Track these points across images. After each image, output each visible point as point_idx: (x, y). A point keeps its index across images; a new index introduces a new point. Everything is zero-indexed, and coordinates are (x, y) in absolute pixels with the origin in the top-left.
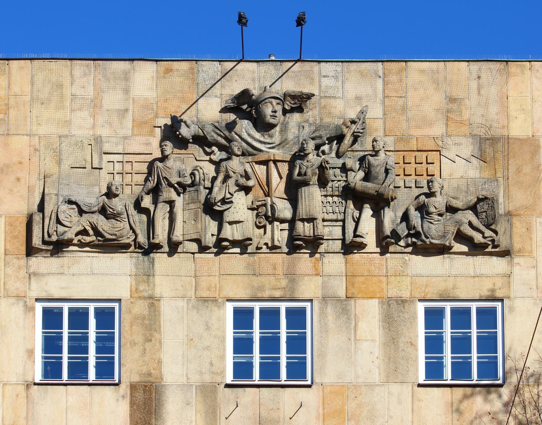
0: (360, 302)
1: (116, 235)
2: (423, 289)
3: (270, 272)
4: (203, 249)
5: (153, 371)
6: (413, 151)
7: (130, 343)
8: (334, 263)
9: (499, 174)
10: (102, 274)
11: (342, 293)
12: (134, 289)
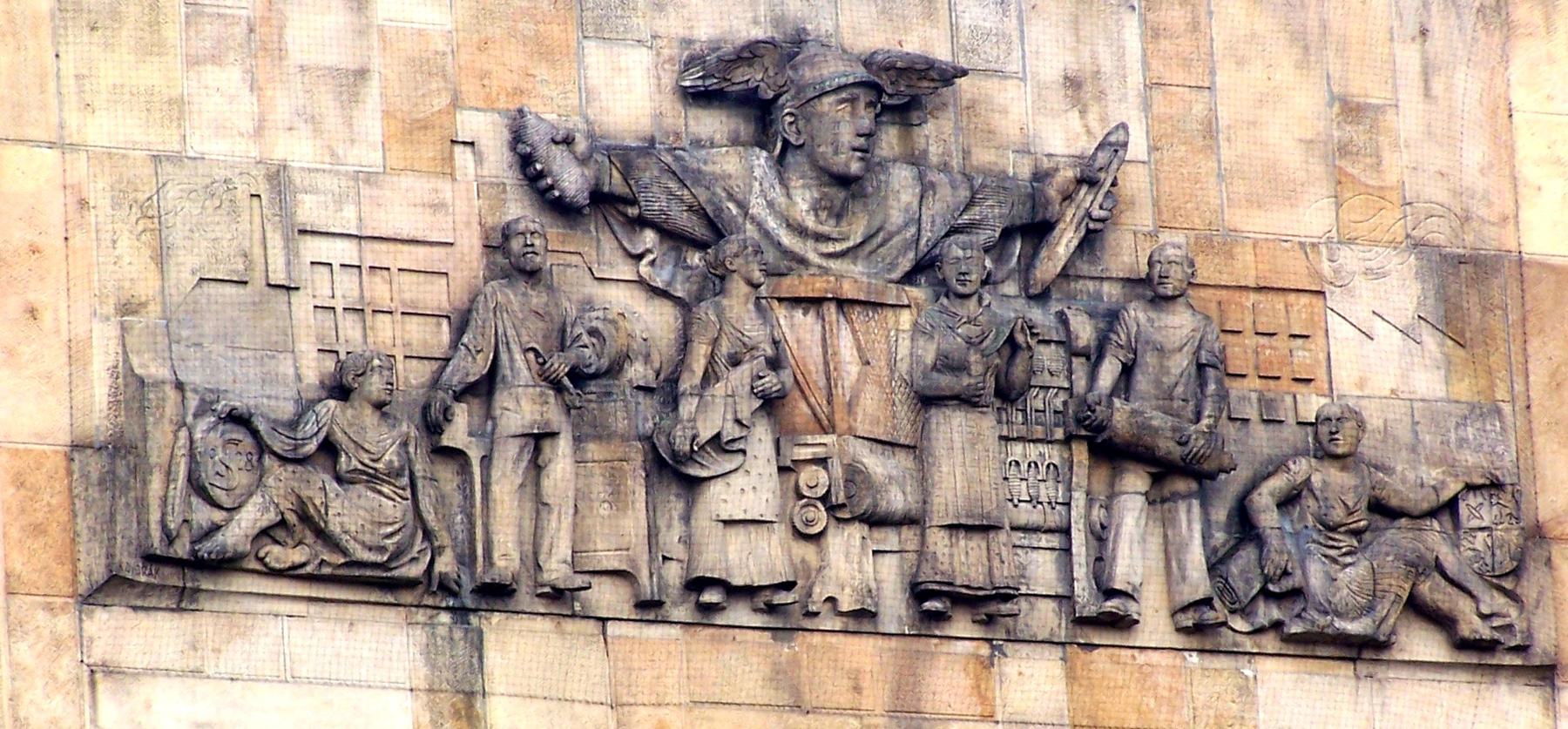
3: (845, 699)
4: (649, 608)
6: (1246, 288)
9: (1502, 393)
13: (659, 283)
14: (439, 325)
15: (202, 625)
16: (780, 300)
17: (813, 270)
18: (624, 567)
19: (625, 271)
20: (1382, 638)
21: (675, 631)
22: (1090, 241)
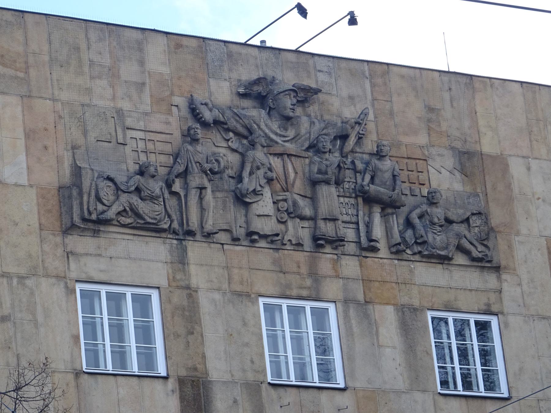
0: (377, 307)
1: (156, 219)
2: (430, 298)
3: (295, 269)
4: (235, 240)
5: (198, 366)
6: (404, 158)
7: (174, 334)
8: (350, 266)
10: (140, 260)
11: (360, 297)
12: (171, 278)
13: (234, 148)
14: (170, 157)
15: (102, 241)
16: (270, 154)
17: (280, 145)
18: (228, 228)
19: (224, 144)
20: (450, 257)
21: (244, 248)
22: (360, 138)
